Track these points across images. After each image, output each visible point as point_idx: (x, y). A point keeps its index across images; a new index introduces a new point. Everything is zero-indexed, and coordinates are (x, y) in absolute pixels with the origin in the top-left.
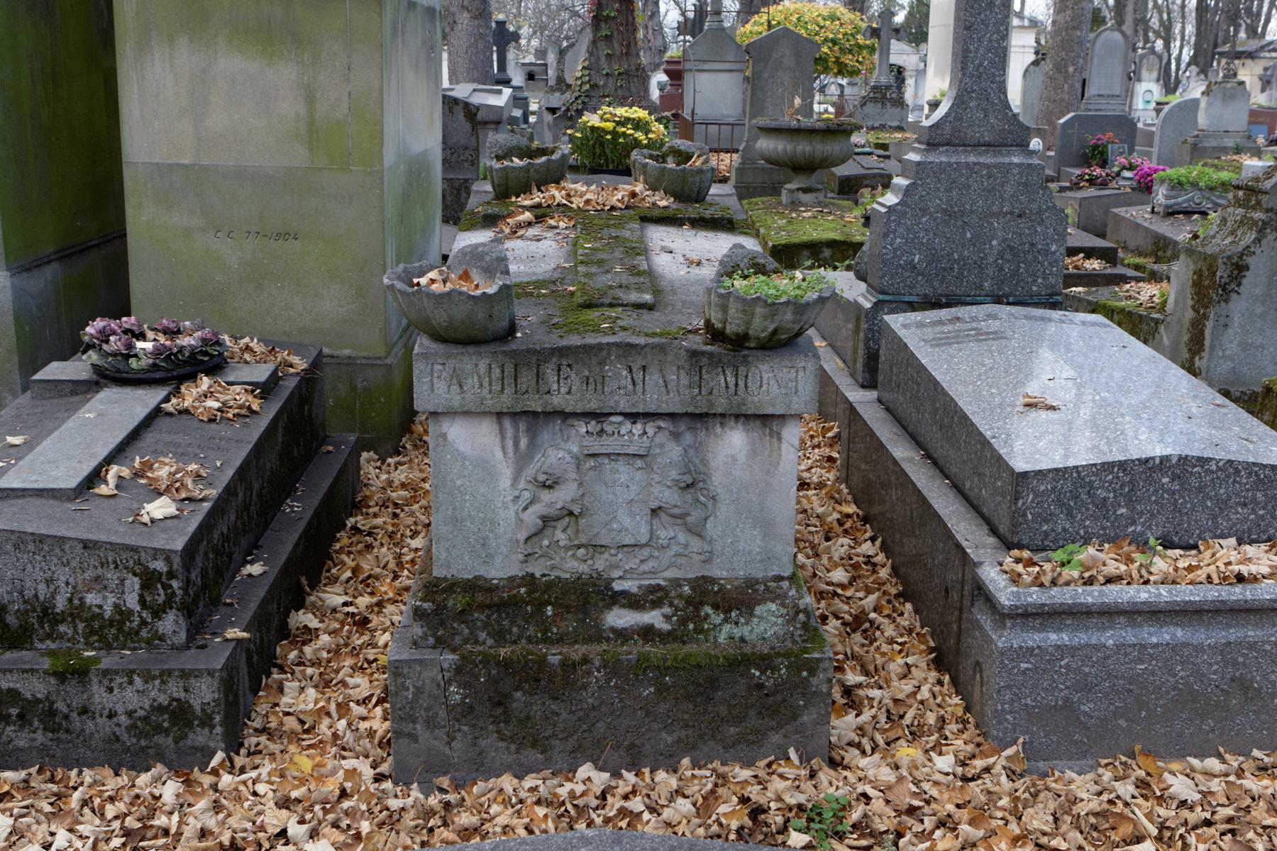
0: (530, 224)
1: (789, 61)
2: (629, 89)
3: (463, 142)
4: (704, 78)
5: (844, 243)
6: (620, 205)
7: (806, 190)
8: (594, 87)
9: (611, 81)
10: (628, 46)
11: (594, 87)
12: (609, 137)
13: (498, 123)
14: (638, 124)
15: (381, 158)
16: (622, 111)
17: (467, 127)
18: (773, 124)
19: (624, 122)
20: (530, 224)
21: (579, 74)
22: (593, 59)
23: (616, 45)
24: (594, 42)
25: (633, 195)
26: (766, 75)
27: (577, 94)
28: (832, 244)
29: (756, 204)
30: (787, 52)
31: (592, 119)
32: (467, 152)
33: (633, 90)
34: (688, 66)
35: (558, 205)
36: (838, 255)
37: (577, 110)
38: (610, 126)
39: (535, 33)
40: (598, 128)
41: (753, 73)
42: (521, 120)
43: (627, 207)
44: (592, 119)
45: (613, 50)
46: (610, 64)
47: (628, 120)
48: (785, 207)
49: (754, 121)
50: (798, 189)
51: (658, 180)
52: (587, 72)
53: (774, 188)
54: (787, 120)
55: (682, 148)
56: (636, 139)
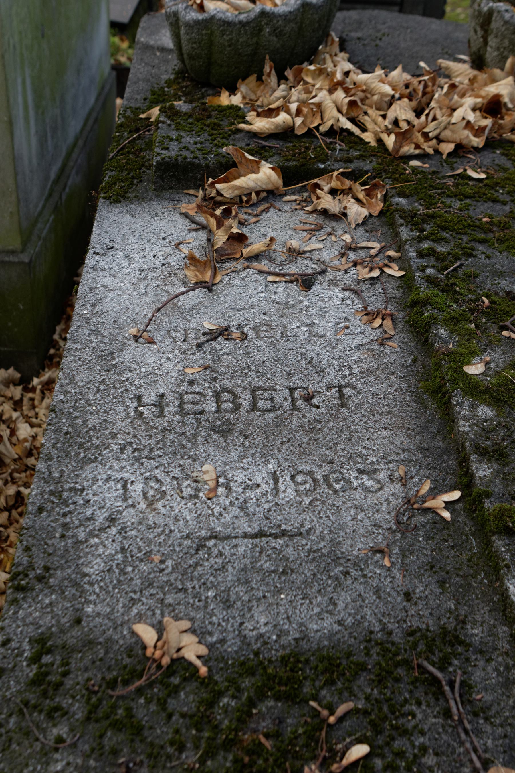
0: (269, 196)
6: (477, 142)
20: (269, 196)
43: (490, 144)
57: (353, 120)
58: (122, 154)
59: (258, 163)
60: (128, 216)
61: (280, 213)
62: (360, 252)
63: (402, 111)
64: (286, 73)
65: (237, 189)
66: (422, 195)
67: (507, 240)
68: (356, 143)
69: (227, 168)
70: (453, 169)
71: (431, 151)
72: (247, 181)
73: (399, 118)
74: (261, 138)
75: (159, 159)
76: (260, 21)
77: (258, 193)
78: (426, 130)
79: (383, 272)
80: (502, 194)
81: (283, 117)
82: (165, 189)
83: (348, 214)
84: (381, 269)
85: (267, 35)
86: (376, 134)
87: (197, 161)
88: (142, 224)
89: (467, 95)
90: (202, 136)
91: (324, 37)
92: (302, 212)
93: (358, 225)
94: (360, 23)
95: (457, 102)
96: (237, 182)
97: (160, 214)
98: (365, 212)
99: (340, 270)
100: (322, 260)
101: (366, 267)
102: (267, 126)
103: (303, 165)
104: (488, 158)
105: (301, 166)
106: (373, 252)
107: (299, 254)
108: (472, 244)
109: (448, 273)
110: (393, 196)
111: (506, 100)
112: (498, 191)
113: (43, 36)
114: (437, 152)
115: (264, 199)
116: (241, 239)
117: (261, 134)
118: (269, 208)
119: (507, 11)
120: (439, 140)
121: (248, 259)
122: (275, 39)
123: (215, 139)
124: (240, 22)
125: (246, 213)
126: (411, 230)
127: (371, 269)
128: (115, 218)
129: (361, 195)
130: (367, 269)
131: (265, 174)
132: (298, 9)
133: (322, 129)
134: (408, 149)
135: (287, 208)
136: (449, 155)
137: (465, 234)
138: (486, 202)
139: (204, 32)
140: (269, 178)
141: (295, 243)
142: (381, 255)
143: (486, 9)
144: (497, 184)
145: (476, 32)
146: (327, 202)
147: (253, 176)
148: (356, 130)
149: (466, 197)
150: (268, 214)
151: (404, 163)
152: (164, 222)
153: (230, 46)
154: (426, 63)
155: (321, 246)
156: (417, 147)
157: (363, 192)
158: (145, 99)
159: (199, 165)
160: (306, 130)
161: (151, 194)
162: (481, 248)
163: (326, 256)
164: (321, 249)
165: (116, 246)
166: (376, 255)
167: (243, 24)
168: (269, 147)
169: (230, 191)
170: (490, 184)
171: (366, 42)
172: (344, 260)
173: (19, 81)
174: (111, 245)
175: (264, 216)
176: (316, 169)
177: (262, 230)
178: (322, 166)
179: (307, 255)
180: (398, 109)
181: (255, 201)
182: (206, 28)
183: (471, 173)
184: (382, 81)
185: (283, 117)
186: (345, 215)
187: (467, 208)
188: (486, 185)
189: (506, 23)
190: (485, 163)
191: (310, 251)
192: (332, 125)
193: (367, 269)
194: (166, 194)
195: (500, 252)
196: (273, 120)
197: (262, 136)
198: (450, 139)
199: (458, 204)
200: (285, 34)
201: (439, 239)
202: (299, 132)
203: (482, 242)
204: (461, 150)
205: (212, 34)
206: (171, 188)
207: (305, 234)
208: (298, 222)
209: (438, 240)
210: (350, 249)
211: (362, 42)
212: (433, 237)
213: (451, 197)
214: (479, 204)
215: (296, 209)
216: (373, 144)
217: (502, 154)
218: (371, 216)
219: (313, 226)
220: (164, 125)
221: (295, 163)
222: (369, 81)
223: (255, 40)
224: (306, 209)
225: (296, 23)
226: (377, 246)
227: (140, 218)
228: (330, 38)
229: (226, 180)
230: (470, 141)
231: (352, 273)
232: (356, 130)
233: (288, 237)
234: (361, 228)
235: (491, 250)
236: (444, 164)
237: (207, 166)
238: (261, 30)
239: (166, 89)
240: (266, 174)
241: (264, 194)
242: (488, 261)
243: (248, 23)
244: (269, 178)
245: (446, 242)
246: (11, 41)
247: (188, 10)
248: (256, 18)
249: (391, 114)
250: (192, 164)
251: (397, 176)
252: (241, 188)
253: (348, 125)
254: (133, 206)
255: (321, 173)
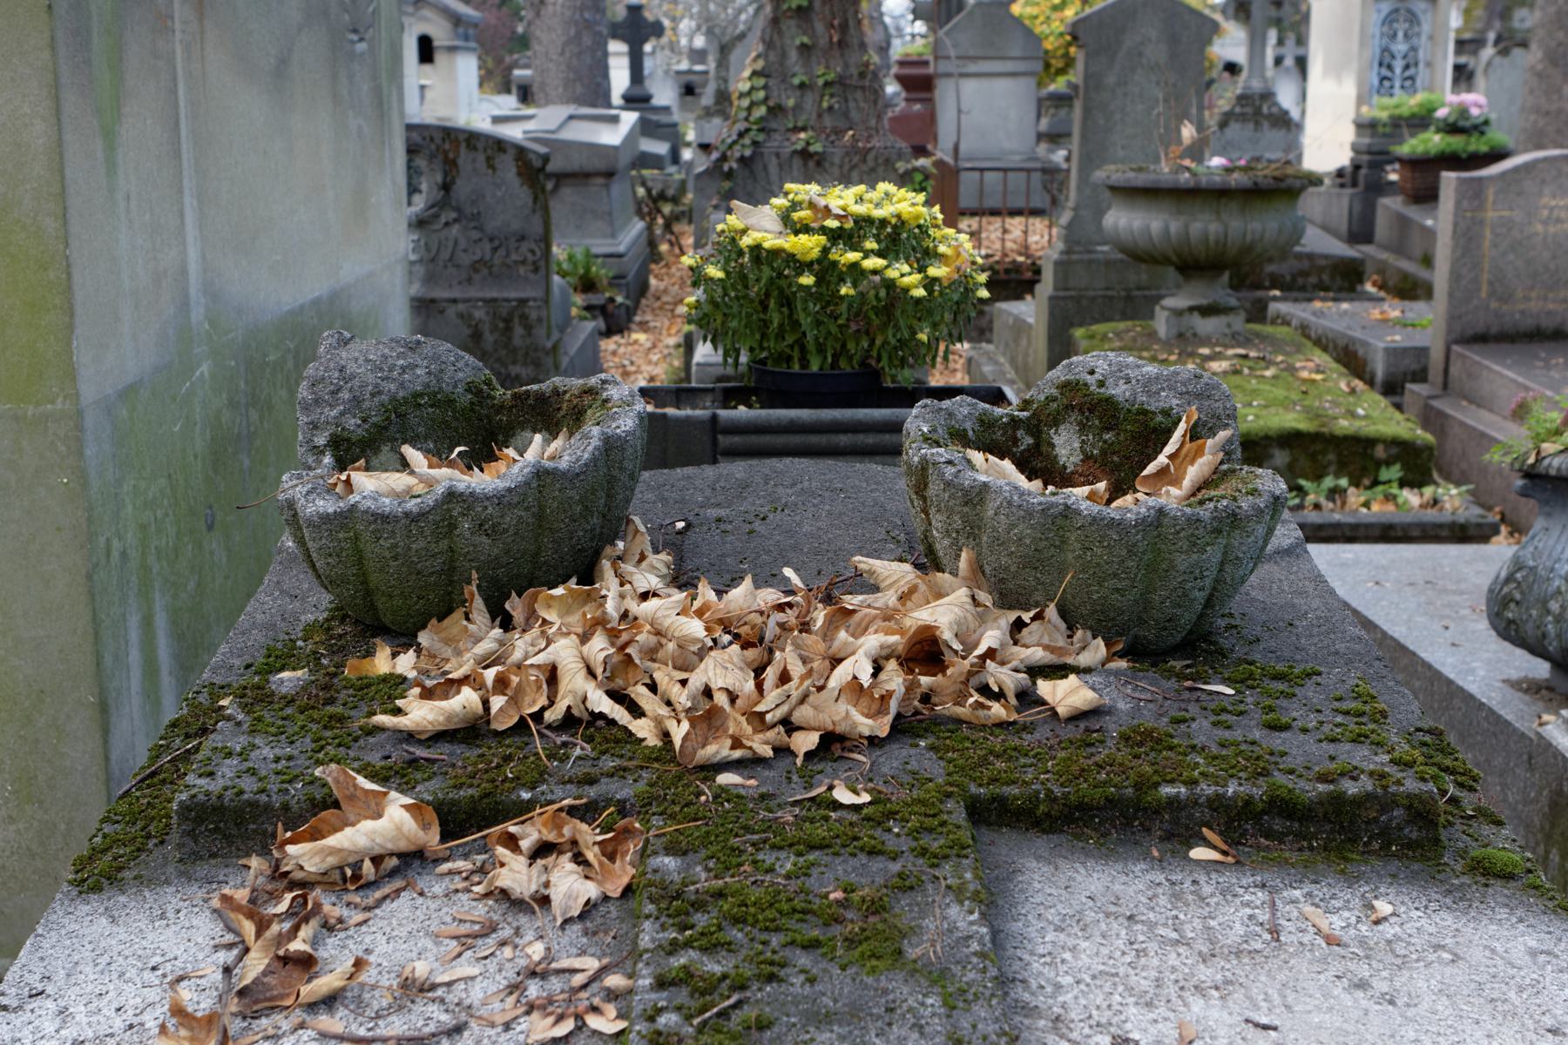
0: (407, 863)
1: (1156, 52)
2: (846, 114)
3: (516, 225)
4: (970, 87)
5: (1316, 437)
6: (865, 725)
7: (1207, 311)
8: (776, 111)
9: (809, 100)
10: (844, 28)
11: (776, 111)
12: (807, 280)
13: (610, 174)
14: (898, 238)
15: (70, 375)
16: (844, 199)
17: (523, 195)
18: (1141, 180)
19: (850, 233)
20: (407, 863)
21: (744, 86)
22: (772, 57)
23: (820, 27)
24: (775, 21)
25: (925, 652)
26: (1111, 80)
27: (741, 126)
28: (1291, 439)
29: (1104, 338)
30: (1153, 34)
31: (759, 225)
32: (525, 246)
33: (854, 115)
34: (943, 67)
35: (569, 721)
36: (1304, 462)
37: (742, 159)
38: (808, 245)
39: (699, 28)
40: (776, 253)
41: (1087, 77)
42: (668, 161)
43: (903, 728)
44: (759, 225)
45: (813, 36)
46: (807, 64)
47: (864, 223)
48: (1167, 345)
49: (1099, 175)
50: (1191, 309)
51: (1033, 561)
52: (761, 82)
53: (1129, 298)
54: (1164, 171)
55: (1119, 391)
56: (890, 285)
57: (618, 696)
58: (149, 786)
59: (385, 794)
60: (104, 921)
61: (420, 900)
62: (554, 979)
63: (724, 671)
64: (507, 606)
65: (330, 854)
66: (713, 848)
67: (867, 939)
68: (617, 741)
69: (321, 810)
70: (809, 786)
71: (767, 751)
72: (358, 836)
73: (713, 686)
74: (420, 742)
75: (184, 797)
76: (449, 510)
77: (377, 860)
78: (760, 708)
79: (581, 1026)
80: (898, 835)
81: (467, 698)
82: (201, 858)
83: (553, 897)
84: (579, 1017)
85: (467, 534)
86: (658, 721)
87: (263, 798)
88: (123, 936)
89: (871, 630)
90: (298, 744)
91: (613, 527)
92: (464, 897)
93: (566, 921)
94: (745, 485)
95: (846, 643)
96: (333, 841)
97: (171, 915)
98: (591, 890)
99: (493, 1025)
100: (467, 1002)
101: (551, 1014)
102: (430, 717)
103: (487, 795)
104: (894, 760)
105: (481, 798)
106: (578, 979)
107: (421, 990)
108: (787, 952)
109: (705, 1022)
110: (655, 853)
111: (947, 635)
112: (889, 830)
113: (210, 527)
114: (782, 751)
115: (393, 873)
116: (306, 963)
117: (420, 733)
118: (404, 889)
119: (950, 462)
120: (789, 726)
121: (312, 1007)
122: (484, 539)
123: (322, 748)
124: (407, 514)
125: (348, 904)
126: (663, 928)
127: (560, 1018)
128: (74, 926)
129: (591, 855)
130: (551, 1019)
131: (391, 819)
132: (527, 484)
133: (550, 716)
134: (718, 749)
135: (438, 889)
136: (809, 755)
137: (777, 930)
138: (854, 855)
139: (341, 535)
140: (399, 828)
141: (421, 969)
142: (595, 987)
143: (916, 459)
144: (891, 814)
145: (912, 502)
146: (516, 874)
147: (367, 825)
148: (619, 713)
149: (812, 847)
150: (395, 904)
151: (704, 780)
152: (169, 932)
153: (395, 558)
154: (796, 570)
155: (474, 970)
156: (737, 743)
157: (596, 848)
158: (248, 667)
159: (268, 807)
160: (516, 719)
161: (170, 869)
162: (803, 960)
163: (476, 994)
164: (473, 978)
165: (50, 990)
166: (584, 987)
167: (412, 518)
168: (426, 760)
169: (317, 859)
170: (880, 814)
171: (729, 527)
172: (511, 1000)
173: (134, 620)
174: (40, 987)
175: (388, 906)
176: (514, 803)
177: (367, 940)
178: (526, 795)
179: (439, 992)
180: (711, 667)
181: (372, 878)
182: (343, 527)
183: (843, 795)
184: (683, 612)
185: (467, 698)
186: (545, 901)
187: (803, 872)
188: (868, 819)
189: (948, 484)
190: (885, 770)
191: (449, 984)
192: (569, 707)
193: (551, 1019)
194: (202, 870)
195: (843, 968)
196: (443, 704)
197: (423, 737)
198: (812, 723)
199: (788, 863)
200: (506, 531)
201: (715, 946)
202: (501, 725)
203: (811, 945)
204: (833, 743)
205: (357, 538)
206: (213, 856)
207: (454, 943)
208: (448, 919)
209: (711, 947)
210: (533, 974)
211: (723, 526)
212: (704, 942)
213: (781, 848)
214: (838, 860)
215: (457, 891)
216: (653, 741)
217: (932, 748)
218: (606, 898)
219: (477, 927)
220: (229, 724)
221: (470, 791)
222: (659, 614)
223: (444, 544)
224: (476, 889)
225: (527, 509)
226: (592, 964)
227: (126, 924)
228: (631, 527)
229: (315, 835)
230: (854, 725)
231: (519, 1029)
232: (619, 713)
233: (414, 955)
234: (577, 927)
235: (824, 964)
236: (795, 778)
237: (286, 807)
238: (453, 526)
239: (300, 643)
240: (395, 820)
241: (394, 861)
242: (808, 989)
243: (422, 515)
244: (399, 828)
245: (729, 951)
246: (115, 543)
247: (310, 498)
248: (438, 505)
249: (697, 680)
250: (253, 804)
251: (687, 810)
252: (340, 850)
253: (605, 705)
254: (122, 899)
255: (522, 810)
